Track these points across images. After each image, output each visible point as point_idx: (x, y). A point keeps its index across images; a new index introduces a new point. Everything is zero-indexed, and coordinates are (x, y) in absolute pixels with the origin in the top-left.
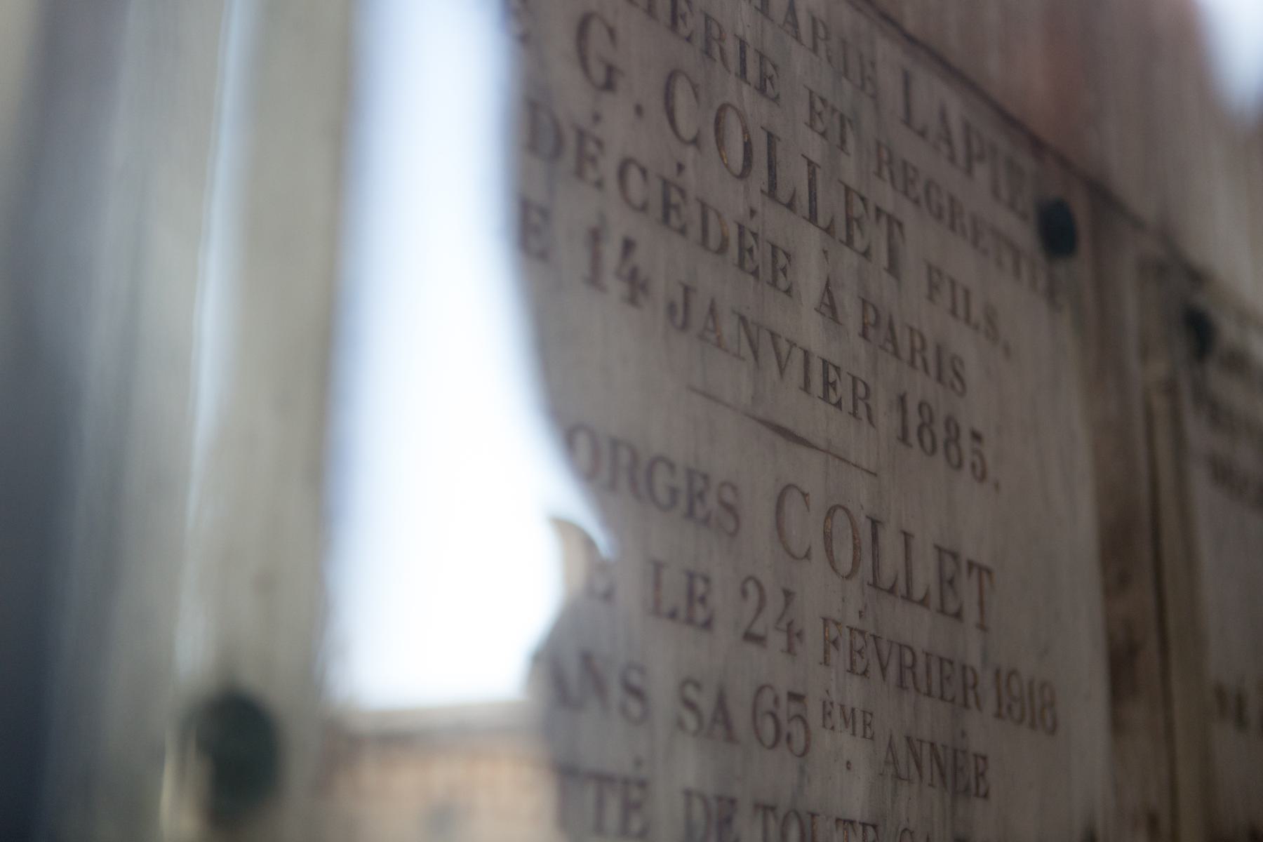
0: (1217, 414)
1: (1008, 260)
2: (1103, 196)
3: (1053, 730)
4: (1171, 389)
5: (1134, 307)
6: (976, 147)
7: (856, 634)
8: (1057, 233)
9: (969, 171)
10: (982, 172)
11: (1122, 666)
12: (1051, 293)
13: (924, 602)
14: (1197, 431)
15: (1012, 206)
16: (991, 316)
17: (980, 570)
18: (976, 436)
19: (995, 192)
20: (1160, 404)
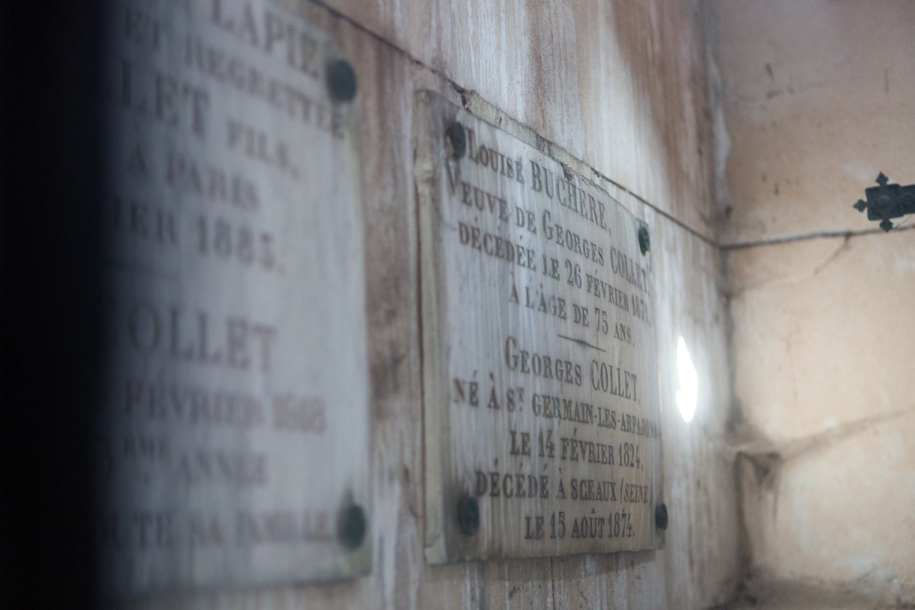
0: (468, 194)
1: (299, 108)
2: (388, 47)
3: (321, 429)
4: (433, 181)
5: (410, 122)
6: (275, 29)
7: (346, 26)
8: (341, 83)
9: (268, 47)
10: (280, 49)
11: (384, 376)
12: (335, 128)
13: (524, 265)
14: (453, 210)
15: (304, 68)
16: (282, 153)
17: (266, 332)
18: (266, 238)
19: (291, 60)
20: (425, 190)
